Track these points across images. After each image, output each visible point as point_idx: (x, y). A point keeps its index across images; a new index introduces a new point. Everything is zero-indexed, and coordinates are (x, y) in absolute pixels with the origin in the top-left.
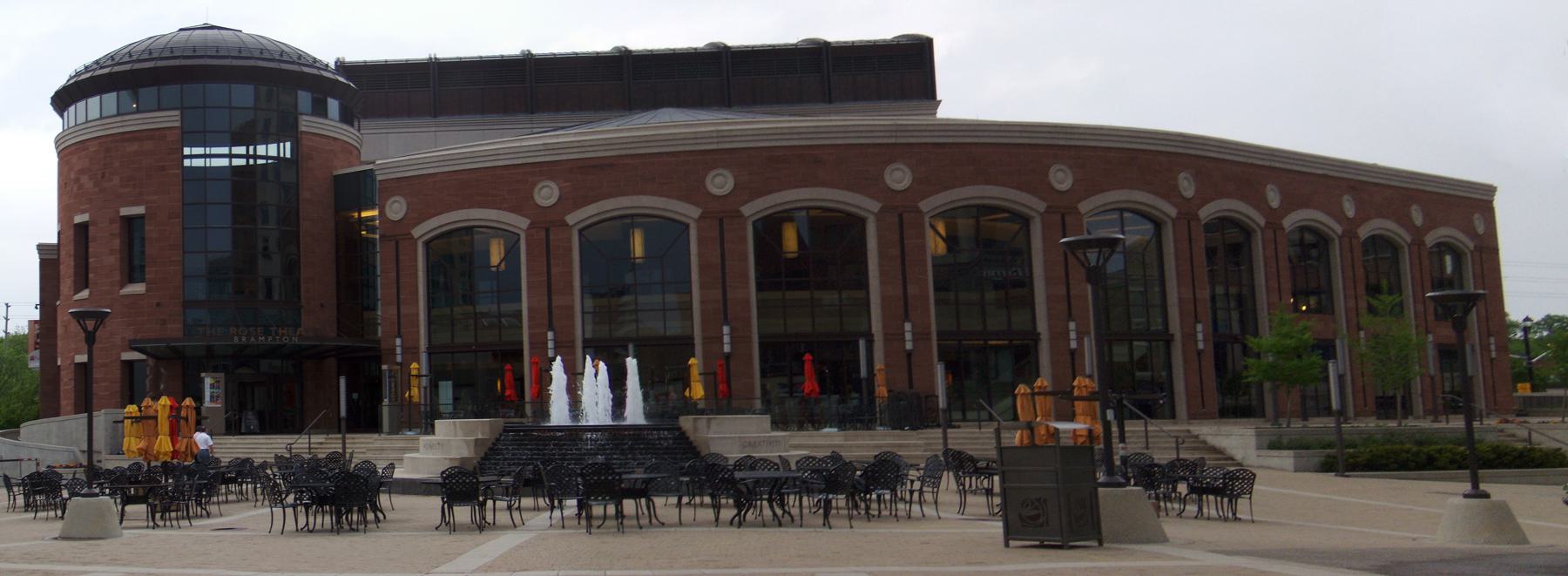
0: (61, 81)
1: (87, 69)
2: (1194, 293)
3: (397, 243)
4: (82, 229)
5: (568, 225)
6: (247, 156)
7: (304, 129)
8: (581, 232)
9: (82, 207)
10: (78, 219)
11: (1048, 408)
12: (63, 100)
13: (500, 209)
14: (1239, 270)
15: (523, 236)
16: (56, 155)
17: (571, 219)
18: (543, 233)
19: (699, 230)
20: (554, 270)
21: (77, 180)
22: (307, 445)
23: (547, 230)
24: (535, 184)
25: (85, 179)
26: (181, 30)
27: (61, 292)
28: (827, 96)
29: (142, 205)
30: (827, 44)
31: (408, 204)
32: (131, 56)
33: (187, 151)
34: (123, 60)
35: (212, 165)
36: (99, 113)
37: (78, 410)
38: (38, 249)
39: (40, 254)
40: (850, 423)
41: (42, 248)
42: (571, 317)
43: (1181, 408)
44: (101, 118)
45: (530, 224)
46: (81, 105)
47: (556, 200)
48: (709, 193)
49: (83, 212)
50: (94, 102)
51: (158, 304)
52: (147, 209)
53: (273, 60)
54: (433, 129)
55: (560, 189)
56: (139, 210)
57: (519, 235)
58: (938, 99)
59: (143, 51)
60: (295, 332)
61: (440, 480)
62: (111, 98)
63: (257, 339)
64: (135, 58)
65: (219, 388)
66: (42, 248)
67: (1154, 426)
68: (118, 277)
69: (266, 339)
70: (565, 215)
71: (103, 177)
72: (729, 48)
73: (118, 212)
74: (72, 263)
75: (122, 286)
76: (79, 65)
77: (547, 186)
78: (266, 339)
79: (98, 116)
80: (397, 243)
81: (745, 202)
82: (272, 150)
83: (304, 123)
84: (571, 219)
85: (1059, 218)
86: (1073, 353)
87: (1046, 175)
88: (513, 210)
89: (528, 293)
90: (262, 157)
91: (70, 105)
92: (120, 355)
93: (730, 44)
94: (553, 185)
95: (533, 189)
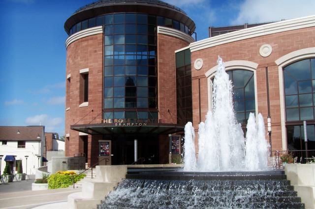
3: (199, 79)
5: (276, 65)
8: (284, 68)
13: (244, 60)
15: (255, 72)
17: (278, 62)
18: (265, 70)
20: (270, 88)
23: (267, 68)
31: (204, 62)
42: (279, 110)
43: (170, 161)
45: (259, 66)
51: (93, 111)
52: (89, 69)
55: (272, 47)
56: (86, 70)
57: (253, 72)
61: (281, 174)
63: (126, 124)
67: (101, 181)
68: (78, 100)
69: (131, 124)
71: (75, 57)
75: (80, 103)
77: (268, 47)
78: (131, 124)
80: (199, 79)
84: (278, 62)
86: (269, 116)
88: (250, 60)
89: (258, 99)
95: (259, 49)
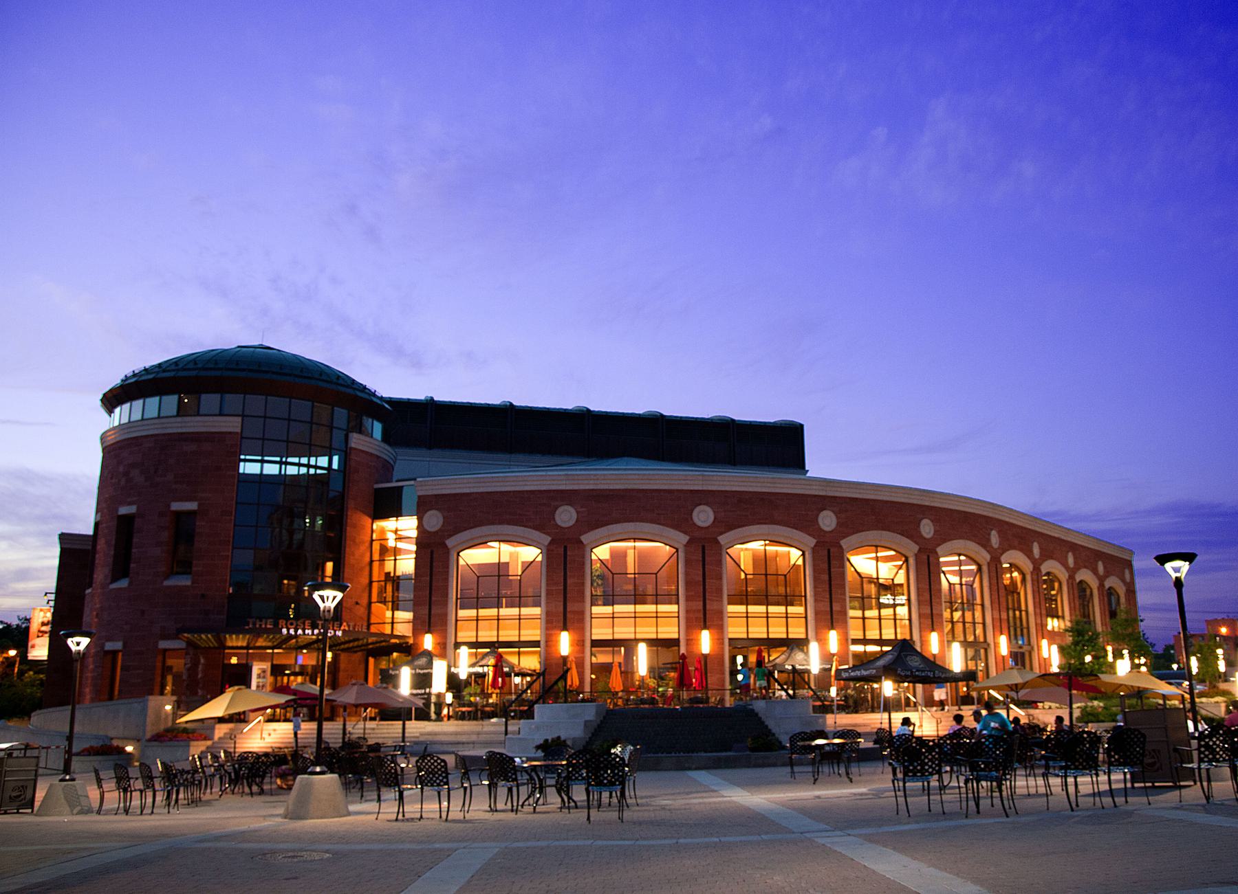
0: (115, 380)
1: (135, 375)
2: (1000, 615)
4: (127, 521)
6: (287, 463)
7: (353, 445)
9: (129, 500)
10: (123, 510)
11: (150, 794)
12: (111, 400)
14: (864, 618)
16: (101, 449)
19: (686, 553)
21: (126, 474)
22: (362, 731)
24: (556, 508)
25: (135, 473)
26: (239, 347)
27: (94, 581)
28: (732, 460)
29: (196, 501)
30: (733, 420)
32: (196, 364)
33: (242, 457)
34: (188, 367)
35: (246, 472)
36: (157, 411)
37: (860, 609)
38: (60, 538)
39: (61, 543)
40: (186, 787)
41: (66, 540)
44: (159, 417)
46: (126, 406)
47: (573, 522)
48: (694, 524)
49: (130, 504)
50: (153, 402)
52: (199, 505)
53: (331, 382)
54: (428, 459)
56: (192, 506)
58: (807, 469)
59: (209, 360)
60: (340, 627)
62: (171, 401)
64: (180, 366)
65: (264, 677)
66: (66, 540)
70: (581, 535)
72: (665, 416)
73: (169, 506)
74: (112, 553)
75: (167, 577)
76: (128, 371)
79: (156, 415)
81: (721, 533)
82: (323, 461)
83: (354, 440)
85: (926, 557)
87: (919, 526)
90: (304, 465)
91: (116, 407)
92: (157, 642)
93: (665, 414)
94: (570, 508)
